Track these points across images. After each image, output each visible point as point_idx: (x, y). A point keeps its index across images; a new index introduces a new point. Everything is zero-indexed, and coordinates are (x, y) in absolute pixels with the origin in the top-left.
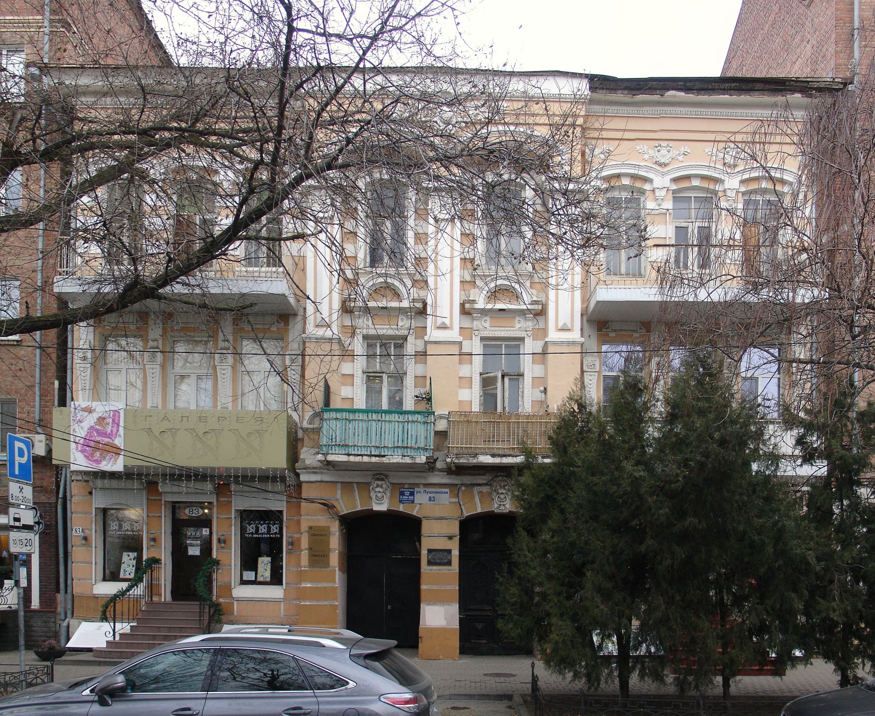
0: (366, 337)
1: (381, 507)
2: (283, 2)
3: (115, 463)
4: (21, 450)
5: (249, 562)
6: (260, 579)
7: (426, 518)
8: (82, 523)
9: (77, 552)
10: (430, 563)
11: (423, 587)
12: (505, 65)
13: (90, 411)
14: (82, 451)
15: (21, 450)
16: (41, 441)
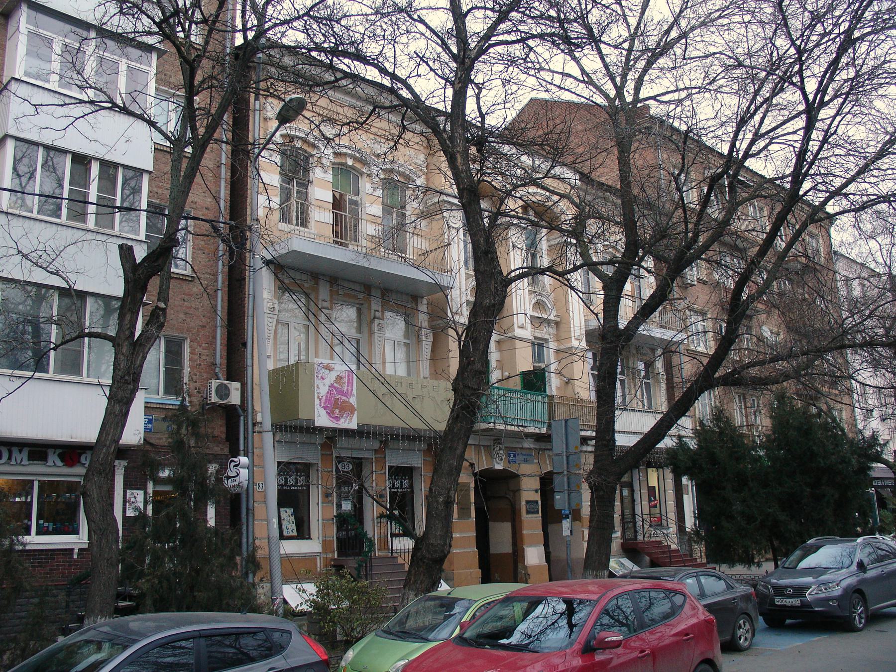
0: (462, 315)
1: (499, 467)
2: (891, 142)
3: (351, 421)
7: (524, 476)
10: (528, 512)
11: (524, 532)
13: (328, 368)
14: (325, 408)
16: (237, 389)
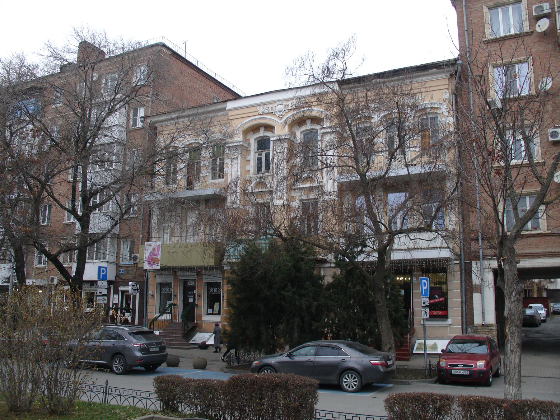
4: (425, 283)
5: (210, 305)
6: (214, 312)
8: (153, 289)
9: (150, 301)
12: (539, 26)
15: (425, 283)
